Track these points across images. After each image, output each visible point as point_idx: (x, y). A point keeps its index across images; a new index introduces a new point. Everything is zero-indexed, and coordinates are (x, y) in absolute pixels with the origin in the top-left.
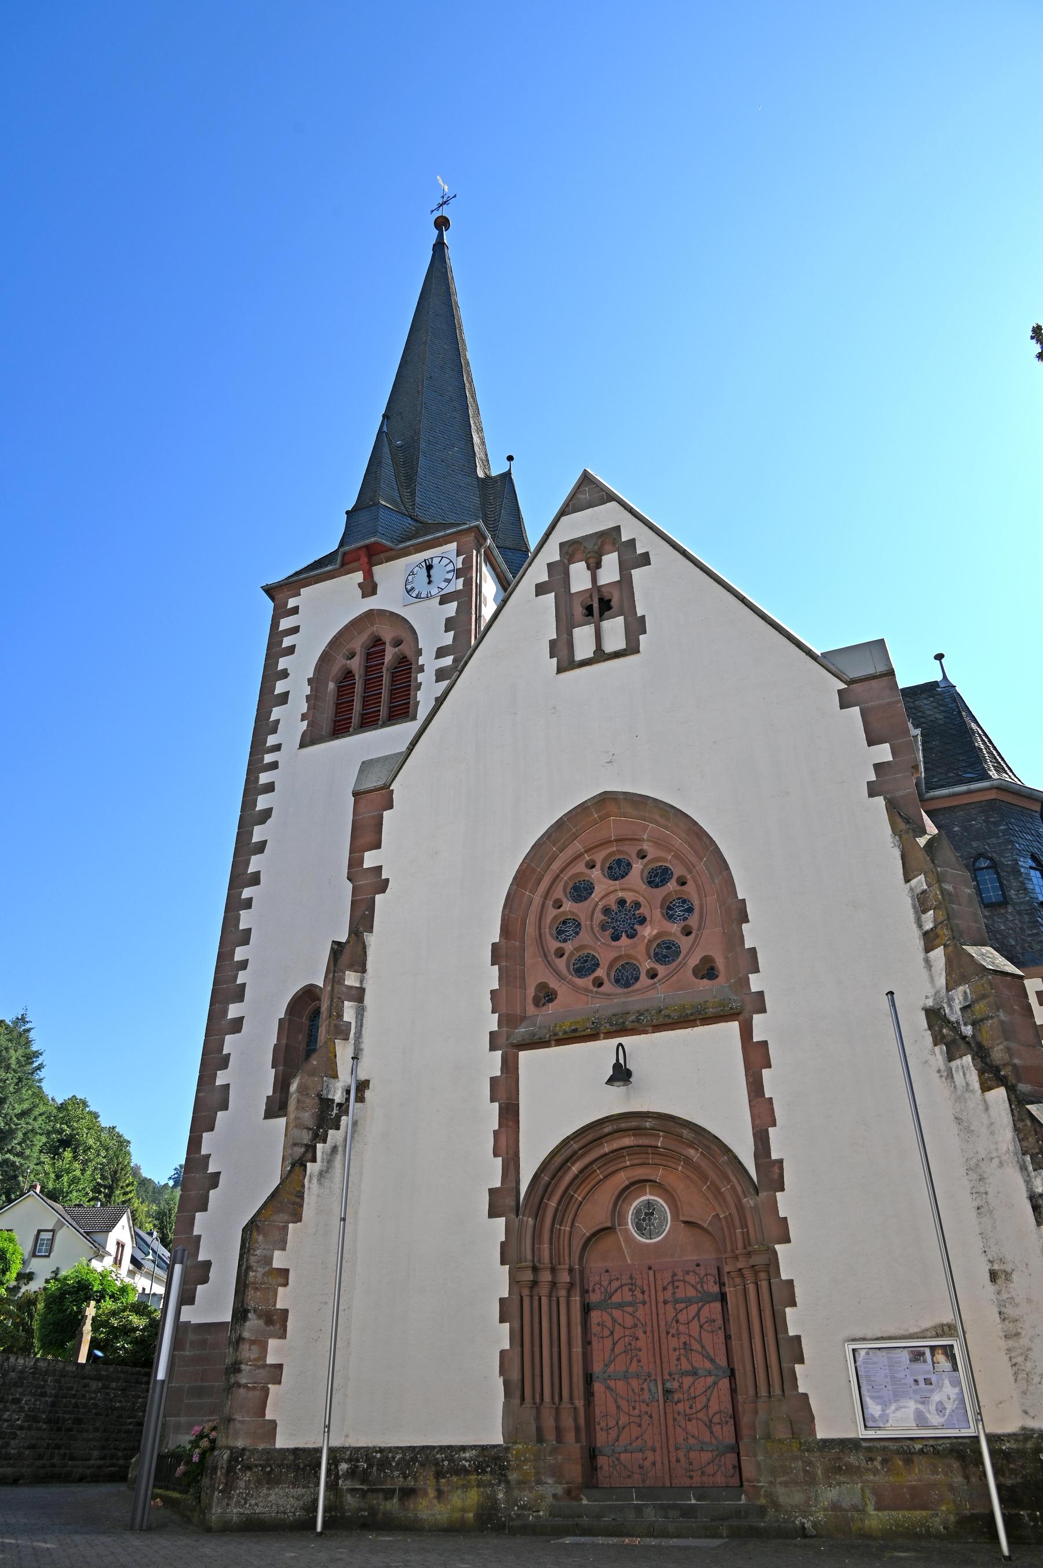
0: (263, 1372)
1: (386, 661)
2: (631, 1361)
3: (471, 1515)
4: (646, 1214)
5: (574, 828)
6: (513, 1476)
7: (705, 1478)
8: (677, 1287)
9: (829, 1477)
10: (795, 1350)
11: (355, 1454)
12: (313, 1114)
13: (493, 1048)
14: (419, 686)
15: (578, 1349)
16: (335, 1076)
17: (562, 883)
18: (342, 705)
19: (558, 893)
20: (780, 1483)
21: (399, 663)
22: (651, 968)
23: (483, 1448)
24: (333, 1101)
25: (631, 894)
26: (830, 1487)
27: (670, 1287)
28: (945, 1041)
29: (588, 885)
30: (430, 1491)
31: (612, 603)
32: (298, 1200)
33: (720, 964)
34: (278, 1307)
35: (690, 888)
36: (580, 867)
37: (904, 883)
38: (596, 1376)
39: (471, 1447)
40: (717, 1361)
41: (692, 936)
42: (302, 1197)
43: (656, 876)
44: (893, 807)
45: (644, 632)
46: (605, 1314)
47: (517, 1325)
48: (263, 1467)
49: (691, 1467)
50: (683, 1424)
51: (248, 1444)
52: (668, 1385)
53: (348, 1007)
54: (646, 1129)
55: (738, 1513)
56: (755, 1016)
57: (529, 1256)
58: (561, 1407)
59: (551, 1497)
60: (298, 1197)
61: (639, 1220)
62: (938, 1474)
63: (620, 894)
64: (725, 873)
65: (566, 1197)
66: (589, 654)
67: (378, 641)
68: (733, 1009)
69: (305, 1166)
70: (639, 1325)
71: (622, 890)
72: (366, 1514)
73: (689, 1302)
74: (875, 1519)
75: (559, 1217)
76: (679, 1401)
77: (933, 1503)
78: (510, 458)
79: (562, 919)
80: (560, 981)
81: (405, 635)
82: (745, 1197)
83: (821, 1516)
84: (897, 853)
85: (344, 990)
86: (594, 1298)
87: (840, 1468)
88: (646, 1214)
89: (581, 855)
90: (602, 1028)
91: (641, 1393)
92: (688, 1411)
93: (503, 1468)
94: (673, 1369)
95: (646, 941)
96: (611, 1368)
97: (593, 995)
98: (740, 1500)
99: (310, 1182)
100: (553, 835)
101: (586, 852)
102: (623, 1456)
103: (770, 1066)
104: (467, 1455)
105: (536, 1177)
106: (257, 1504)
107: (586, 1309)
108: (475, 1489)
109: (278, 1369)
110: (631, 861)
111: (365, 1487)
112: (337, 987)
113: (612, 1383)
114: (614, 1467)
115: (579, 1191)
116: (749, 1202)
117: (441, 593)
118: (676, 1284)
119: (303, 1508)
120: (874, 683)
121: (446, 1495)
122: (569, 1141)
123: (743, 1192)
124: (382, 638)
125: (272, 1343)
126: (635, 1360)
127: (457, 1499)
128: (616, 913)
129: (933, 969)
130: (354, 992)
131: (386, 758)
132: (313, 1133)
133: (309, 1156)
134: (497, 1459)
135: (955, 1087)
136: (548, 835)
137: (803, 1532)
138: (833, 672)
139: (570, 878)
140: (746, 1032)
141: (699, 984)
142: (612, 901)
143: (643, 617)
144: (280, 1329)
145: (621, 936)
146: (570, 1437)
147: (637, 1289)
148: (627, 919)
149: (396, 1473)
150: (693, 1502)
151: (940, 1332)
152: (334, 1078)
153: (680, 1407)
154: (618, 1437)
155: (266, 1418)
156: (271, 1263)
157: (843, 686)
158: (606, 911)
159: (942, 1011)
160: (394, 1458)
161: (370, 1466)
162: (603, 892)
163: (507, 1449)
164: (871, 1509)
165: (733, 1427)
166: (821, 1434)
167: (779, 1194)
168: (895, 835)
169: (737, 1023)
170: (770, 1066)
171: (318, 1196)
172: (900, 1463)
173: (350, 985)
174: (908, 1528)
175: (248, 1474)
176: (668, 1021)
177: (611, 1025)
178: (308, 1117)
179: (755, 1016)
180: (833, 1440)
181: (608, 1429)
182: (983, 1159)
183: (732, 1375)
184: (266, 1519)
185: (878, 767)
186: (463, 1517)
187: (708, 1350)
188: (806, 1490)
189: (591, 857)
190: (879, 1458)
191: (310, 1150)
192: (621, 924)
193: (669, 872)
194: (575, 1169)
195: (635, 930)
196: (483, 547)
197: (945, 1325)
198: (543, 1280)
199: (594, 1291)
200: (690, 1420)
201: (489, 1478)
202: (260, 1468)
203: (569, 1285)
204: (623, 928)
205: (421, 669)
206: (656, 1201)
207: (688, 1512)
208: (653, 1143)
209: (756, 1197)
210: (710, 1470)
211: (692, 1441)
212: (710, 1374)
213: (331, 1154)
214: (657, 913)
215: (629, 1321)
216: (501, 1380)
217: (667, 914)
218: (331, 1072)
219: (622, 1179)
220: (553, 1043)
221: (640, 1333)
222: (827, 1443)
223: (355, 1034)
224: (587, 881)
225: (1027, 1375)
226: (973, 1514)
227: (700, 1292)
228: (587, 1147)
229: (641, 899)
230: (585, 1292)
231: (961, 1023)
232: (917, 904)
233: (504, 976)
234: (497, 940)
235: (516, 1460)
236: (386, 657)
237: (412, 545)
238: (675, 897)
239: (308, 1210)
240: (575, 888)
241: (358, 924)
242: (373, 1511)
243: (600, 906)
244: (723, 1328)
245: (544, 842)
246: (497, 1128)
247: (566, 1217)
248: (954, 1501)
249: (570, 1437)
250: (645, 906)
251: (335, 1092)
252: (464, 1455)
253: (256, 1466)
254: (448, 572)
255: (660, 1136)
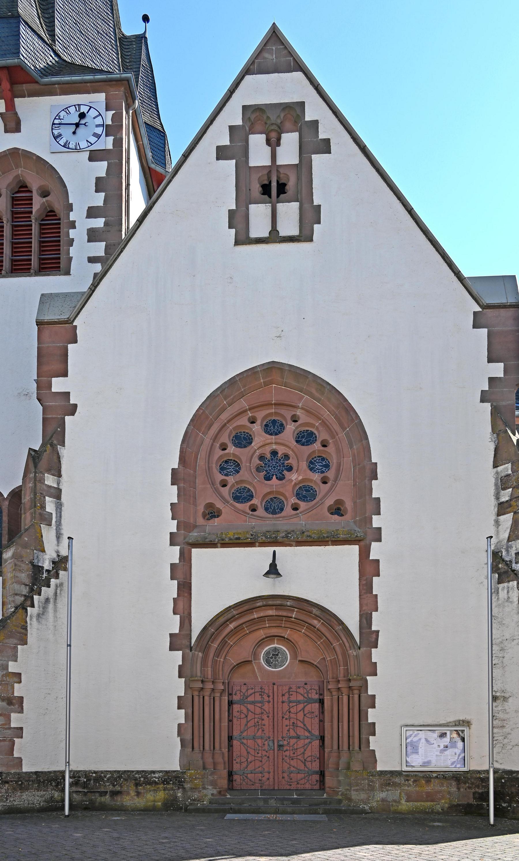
0: (9, 732)
1: (34, 210)
2: (258, 731)
3: (160, 804)
4: (273, 655)
5: (243, 388)
6: (187, 786)
7: (299, 786)
8: (292, 695)
9: (382, 788)
10: (372, 729)
11: (76, 774)
12: (28, 575)
13: (172, 543)
14: (71, 242)
15: (225, 723)
16: (43, 551)
17: (228, 431)
18: (163, 165)
19: (225, 438)
20: (354, 790)
21: (47, 216)
22: (295, 503)
23: (167, 772)
24: (42, 568)
25: (283, 447)
26: (382, 792)
27: (287, 695)
28: (499, 571)
29: (247, 436)
30: (131, 792)
31: (287, 187)
32: (23, 631)
33: (349, 505)
34: (16, 695)
35: (331, 449)
36: (244, 421)
37: (492, 468)
38: (235, 737)
39: (158, 771)
40: (313, 732)
41: (329, 485)
42: (26, 629)
43: (303, 437)
44: (495, 412)
45: (319, 222)
46: (242, 706)
47: (190, 711)
48: (17, 782)
49: (291, 781)
50: (288, 761)
51: (4, 770)
52: (281, 743)
53: (49, 502)
54: (287, 606)
55: (325, 803)
56: (373, 543)
57: (199, 674)
58: (214, 752)
59: (210, 795)
60: (23, 629)
61: (269, 658)
62: (443, 787)
63: (274, 447)
64: (364, 442)
65: (224, 643)
66: (264, 233)
67: (23, 187)
68: (358, 537)
69: (27, 610)
70: (265, 713)
71: (276, 443)
72: (88, 803)
73: (299, 702)
74: (404, 806)
75: (218, 653)
76: (287, 750)
77: (438, 799)
78: (146, 19)
79: (225, 459)
80: (225, 504)
81: (52, 186)
82: (351, 650)
83: (375, 804)
84: (492, 446)
85: (45, 488)
86: (235, 698)
87: (389, 784)
88: (273, 655)
89: (245, 411)
90: (260, 539)
91: (263, 746)
92: (292, 755)
93: (180, 782)
94: (284, 735)
95: (293, 483)
96: (245, 734)
97: (250, 516)
98: (323, 796)
99: (31, 620)
100: (226, 389)
101: (250, 409)
102: (249, 775)
103: (379, 575)
104: (157, 775)
105: (205, 629)
106: (14, 801)
107: (230, 703)
108: (163, 791)
109: (20, 730)
110: (284, 423)
111: (86, 790)
112: (38, 485)
113: (245, 741)
114: (244, 780)
115: (231, 639)
116: (353, 653)
117: (90, 148)
118: (291, 693)
119: (45, 801)
120: (502, 311)
121: (142, 794)
122: (231, 609)
123: (350, 647)
124: (28, 185)
125: (14, 716)
126: (260, 730)
127: (150, 796)
128: (269, 461)
129: (500, 527)
130: (52, 491)
131: (66, 295)
132: (29, 588)
133: (29, 603)
134: (176, 777)
135: (498, 599)
136: (221, 389)
137: (363, 812)
138: (474, 295)
139: (234, 428)
140: (364, 553)
141: (332, 518)
142: (267, 451)
143: (319, 206)
144: (18, 708)
145: (272, 478)
146: (221, 767)
147: (265, 694)
148: (277, 466)
149: (108, 784)
150: (295, 797)
151: (457, 723)
152: (42, 552)
153: (287, 753)
154: (247, 766)
155: (14, 756)
156: (8, 669)
157: (478, 309)
158: (262, 458)
159: (500, 554)
160: (105, 777)
161: (89, 780)
162: (261, 443)
163: (184, 773)
164: (403, 802)
165: (319, 763)
166: (380, 768)
167: (373, 650)
168: (494, 433)
169: (357, 547)
170: (379, 575)
171: (38, 629)
172: (424, 782)
173: (50, 485)
174: (422, 810)
175: (7, 785)
176: (309, 539)
177: (266, 538)
178: (25, 576)
179: (373, 543)
180: (386, 771)
181: (241, 763)
182: (507, 640)
183: (322, 739)
184: (21, 808)
185: (492, 380)
186: (154, 804)
187: (308, 727)
188: (368, 793)
189: (253, 414)
190: (412, 780)
191: (29, 599)
192: (272, 469)
193: (314, 436)
194: (232, 626)
195: (283, 475)
196: (131, 108)
197: (461, 720)
198: (206, 687)
199: (236, 694)
200: (292, 759)
201: (171, 787)
202: (14, 782)
203: (222, 691)
204: (274, 472)
205: (73, 225)
206: (281, 648)
207: (295, 802)
208: (290, 615)
209: (358, 650)
210: (302, 782)
211: (292, 769)
212: (308, 738)
213: (45, 603)
214: (304, 465)
215: (258, 710)
216: (179, 739)
217: (309, 466)
218: (39, 547)
219: (261, 634)
220: (219, 545)
221: (265, 717)
222: (382, 773)
223: (56, 522)
224: (247, 433)
225: (503, 745)
226: (458, 804)
227: (306, 698)
228: (242, 614)
229: (290, 453)
230: (230, 694)
231: (514, 561)
232: (499, 483)
233: (182, 494)
234: (176, 466)
235: (189, 778)
236: (33, 206)
237: (58, 83)
238: (317, 455)
239: (30, 639)
240: (236, 437)
241: (52, 437)
242: (92, 802)
243: (258, 453)
244: (318, 716)
245: (218, 395)
246: (176, 596)
247: (221, 653)
248: (449, 798)
249: (221, 767)
250: (293, 458)
251: (43, 561)
252: (154, 775)
253: (12, 781)
254: (97, 126)
255: (295, 611)
